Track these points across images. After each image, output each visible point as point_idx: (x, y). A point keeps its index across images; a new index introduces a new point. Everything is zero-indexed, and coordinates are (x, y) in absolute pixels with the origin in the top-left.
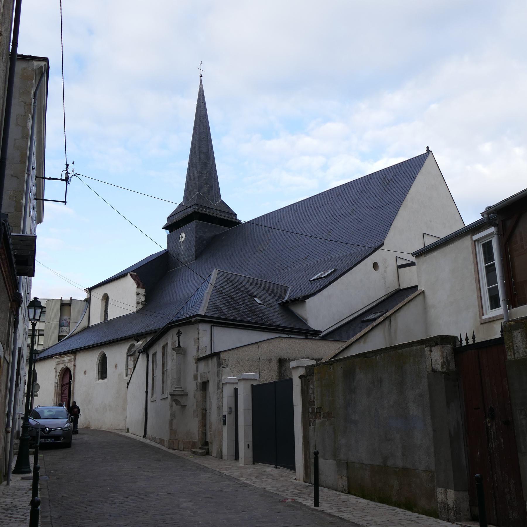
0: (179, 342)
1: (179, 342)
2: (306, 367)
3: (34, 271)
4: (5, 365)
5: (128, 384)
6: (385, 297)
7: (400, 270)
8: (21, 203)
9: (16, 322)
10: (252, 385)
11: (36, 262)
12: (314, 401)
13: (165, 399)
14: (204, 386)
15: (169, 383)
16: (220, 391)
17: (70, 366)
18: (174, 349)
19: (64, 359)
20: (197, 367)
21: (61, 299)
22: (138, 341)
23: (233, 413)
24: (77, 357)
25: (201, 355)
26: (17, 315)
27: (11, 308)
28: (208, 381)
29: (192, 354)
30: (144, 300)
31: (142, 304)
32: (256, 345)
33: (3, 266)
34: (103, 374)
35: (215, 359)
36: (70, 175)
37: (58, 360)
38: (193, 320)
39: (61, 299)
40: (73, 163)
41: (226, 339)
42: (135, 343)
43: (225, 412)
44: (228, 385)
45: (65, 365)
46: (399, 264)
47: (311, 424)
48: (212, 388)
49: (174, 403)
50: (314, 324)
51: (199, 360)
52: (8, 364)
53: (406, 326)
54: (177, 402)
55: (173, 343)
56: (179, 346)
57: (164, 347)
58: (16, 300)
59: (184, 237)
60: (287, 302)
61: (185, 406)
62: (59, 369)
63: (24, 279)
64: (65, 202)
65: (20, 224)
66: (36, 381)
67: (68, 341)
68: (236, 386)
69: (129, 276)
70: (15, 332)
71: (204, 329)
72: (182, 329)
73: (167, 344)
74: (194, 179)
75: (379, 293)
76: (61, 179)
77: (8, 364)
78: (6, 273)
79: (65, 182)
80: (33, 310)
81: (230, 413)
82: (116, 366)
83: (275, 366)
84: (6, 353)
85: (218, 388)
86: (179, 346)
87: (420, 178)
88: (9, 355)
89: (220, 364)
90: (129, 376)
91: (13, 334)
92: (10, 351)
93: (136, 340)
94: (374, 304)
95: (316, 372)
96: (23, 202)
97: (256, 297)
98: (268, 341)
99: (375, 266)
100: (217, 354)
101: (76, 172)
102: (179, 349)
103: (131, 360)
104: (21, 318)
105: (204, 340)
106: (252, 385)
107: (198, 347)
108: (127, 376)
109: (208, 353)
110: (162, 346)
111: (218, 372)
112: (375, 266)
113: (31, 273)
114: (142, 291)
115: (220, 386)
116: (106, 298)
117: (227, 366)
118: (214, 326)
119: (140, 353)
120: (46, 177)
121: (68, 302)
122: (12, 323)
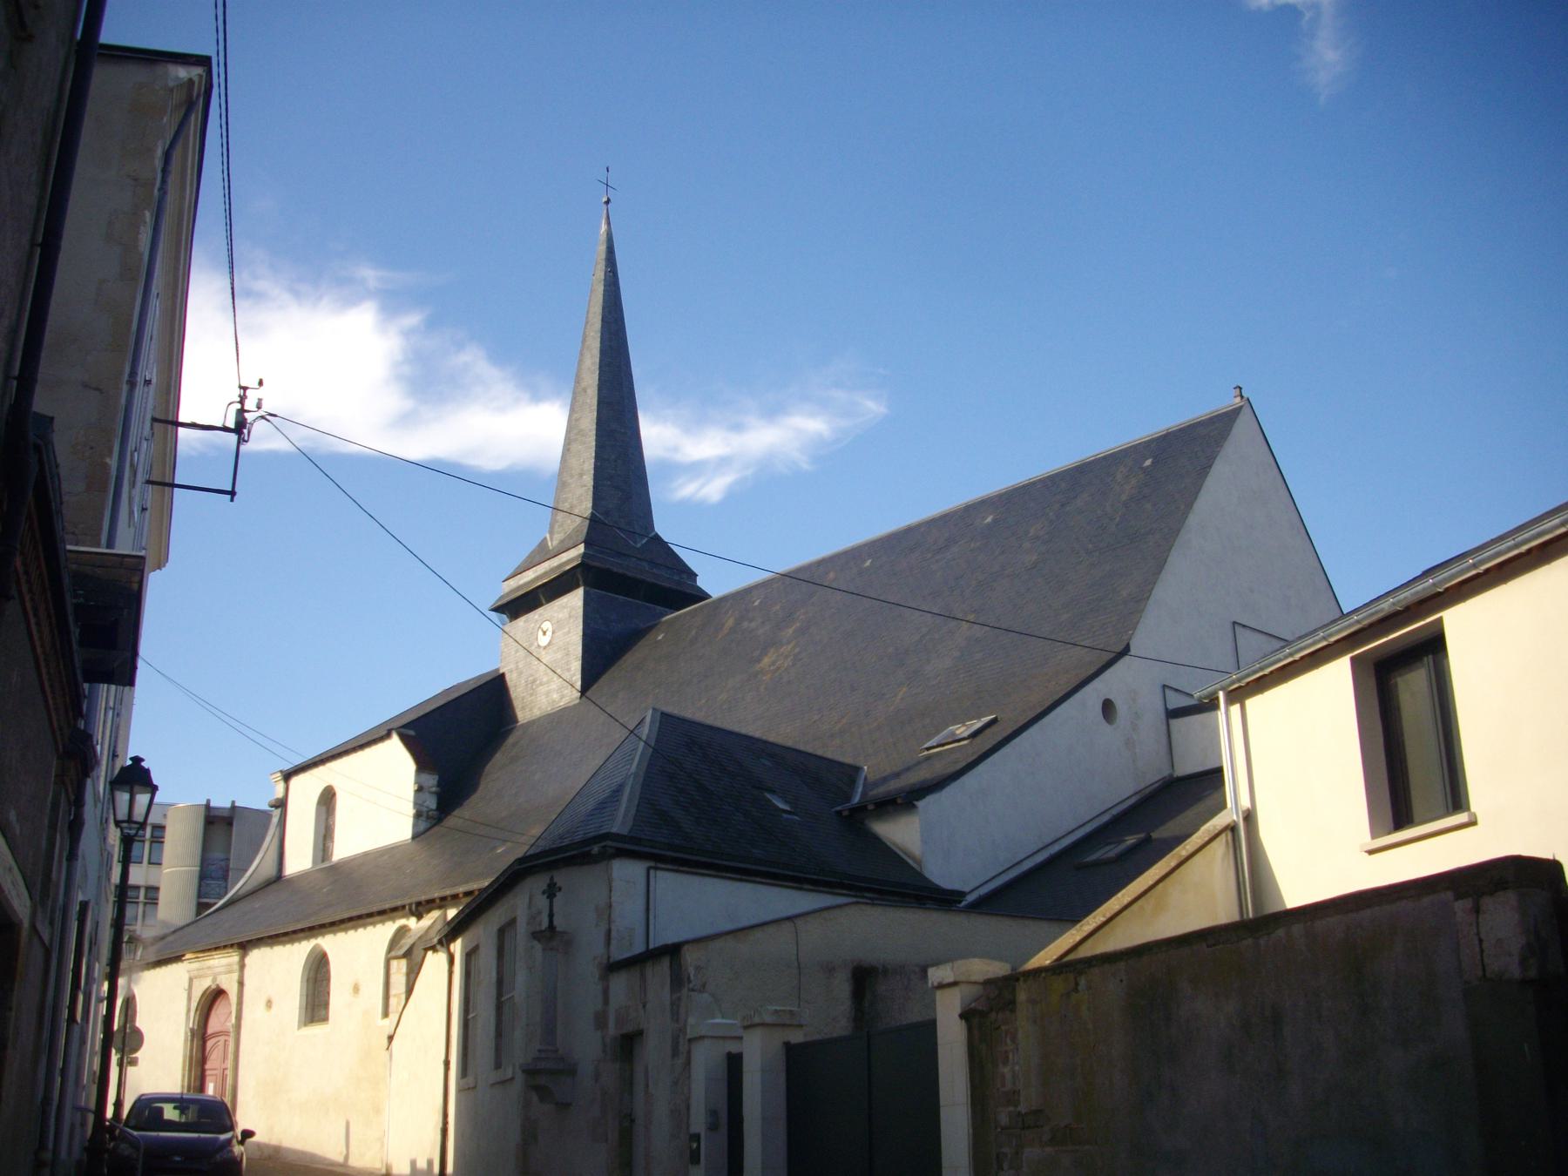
0: (551, 916)
1: (551, 916)
2: (988, 983)
3: (133, 669)
4: (37, 953)
5: (391, 1038)
6: (1133, 800)
7: (1177, 724)
8: (106, 467)
9: (76, 827)
10: (788, 1047)
11: (140, 664)
12: (1016, 1092)
13: (503, 1082)
14: (628, 1044)
15: (518, 1035)
16: (680, 1061)
17: (229, 984)
18: (536, 935)
19: (211, 963)
20: (606, 992)
21: (208, 806)
22: (419, 917)
23: (724, 1130)
24: (248, 960)
25: (618, 954)
26: (79, 802)
27: (61, 778)
28: (640, 1033)
29: (590, 951)
30: (434, 806)
31: (428, 818)
32: (788, 926)
33: (35, 615)
34: (316, 1005)
35: (666, 962)
36: (249, 417)
37: (195, 965)
38: (596, 849)
39: (208, 806)
40: (261, 383)
41: (693, 904)
42: (412, 922)
43: (698, 1123)
44: (707, 1042)
45: (214, 980)
46: (1170, 707)
47: (1005, 1166)
48: (653, 1052)
49: (535, 1098)
50: (941, 874)
51: (613, 967)
52: (48, 953)
53: (1186, 896)
54: (543, 1092)
55: (532, 918)
56: (551, 926)
57: (502, 932)
58: (77, 754)
59: (549, 633)
60: (861, 809)
61: (568, 1105)
62: (197, 994)
63: (106, 693)
64: (232, 493)
65: (101, 529)
66: (134, 1020)
67: (224, 914)
68: (733, 1047)
69: (395, 739)
70: (72, 856)
71: (627, 873)
72: (561, 877)
73: (512, 922)
74: (581, 475)
75: (1117, 786)
76: (225, 429)
77: (48, 953)
78: (42, 646)
79: (233, 437)
80: (126, 796)
81: (713, 1127)
82: (356, 989)
83: (842, 987)
84: (39, 915)
85: (675, 1053)
86: (551, 926)
87: (1221, 471)
88: (52, 923)
89: (678, 980)
90: (393, 1017)
91: (65, 863)
92: (53, 911)
93: (413, 914)
94: (1106, 818)
95: (1022, 996)
96: (113, 463)
97: (773, 792)
98: (825, 914)
99: (1108, 708)
100: (673, 951)
101: (266, 407)
102: (548, 935)
103: (400, 968)
104: (90, 813)
105: (628, 911)
106: (788, 1047)
107: (609, 931)
108: (386, 1014)
109: (639, 948)
110: (495, 928)
111: (675, 1005)
112: (1108, 708)
113: (125, 675)
114: (431, 780)
115: (681, 1046)
116: (328, 799)
117: (704, 986)
118: (656, 868)
119: (426, 950)
120: (181, 419)
121: (226, 814)
122: (62, 825)
